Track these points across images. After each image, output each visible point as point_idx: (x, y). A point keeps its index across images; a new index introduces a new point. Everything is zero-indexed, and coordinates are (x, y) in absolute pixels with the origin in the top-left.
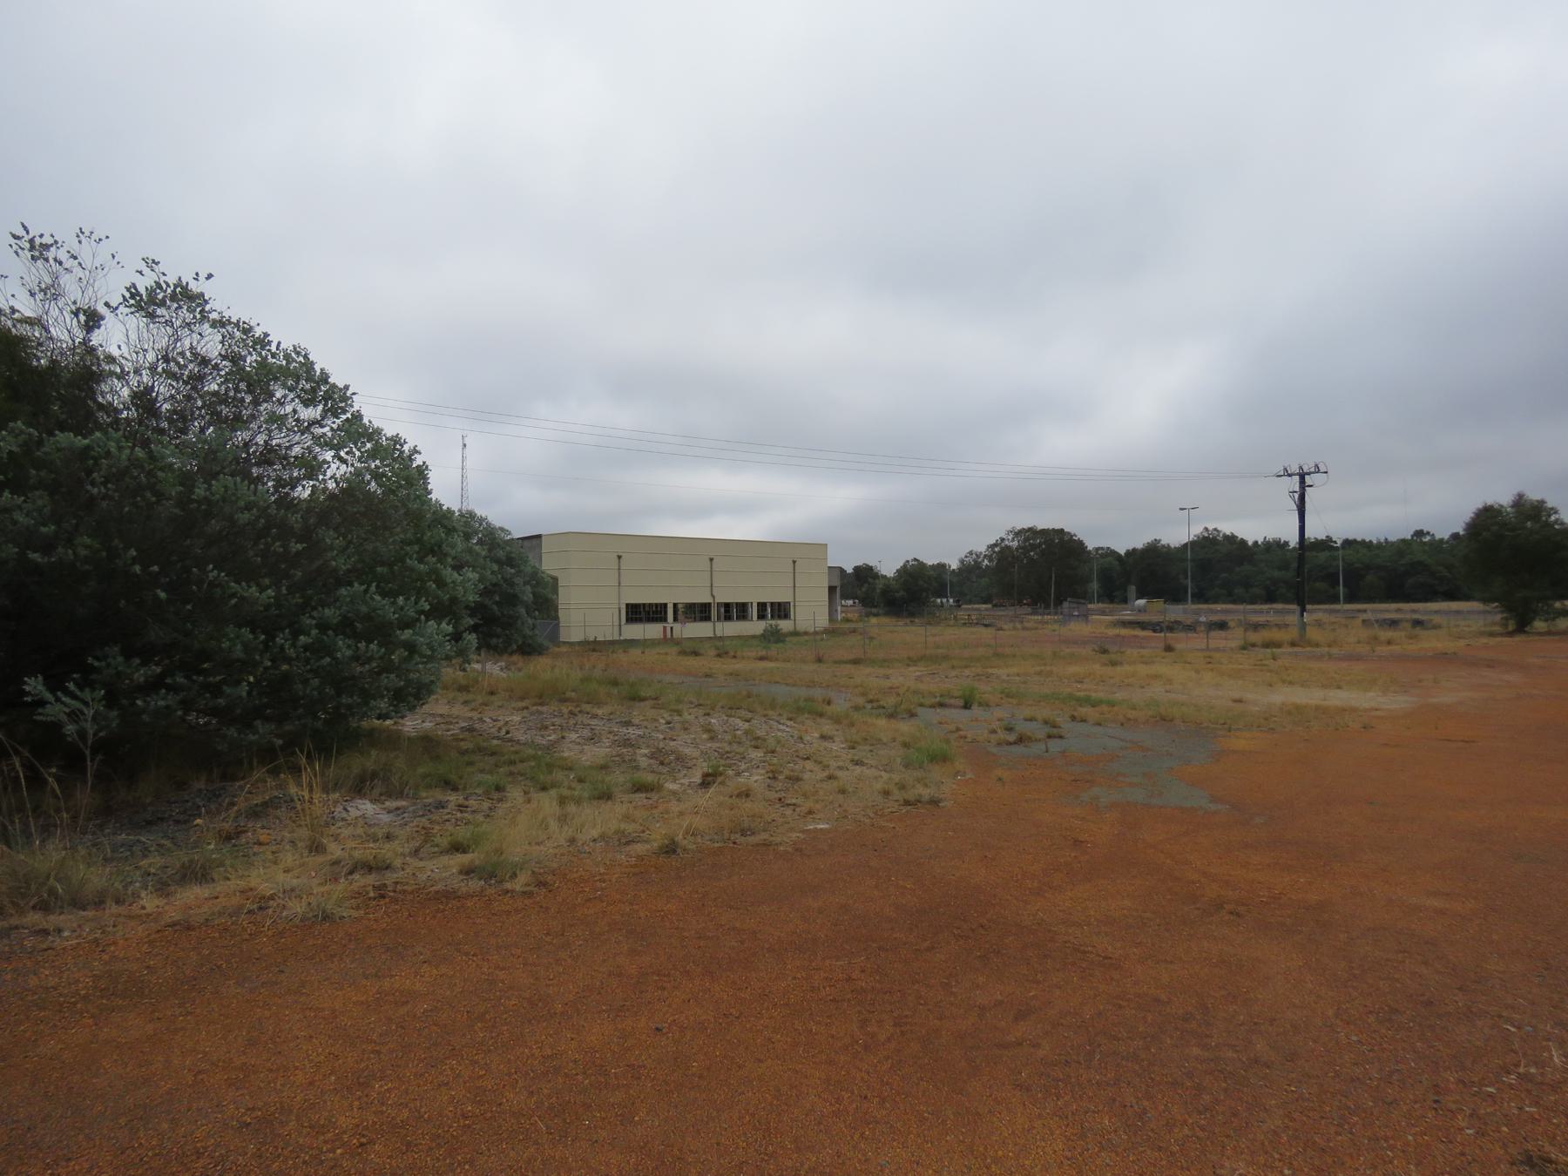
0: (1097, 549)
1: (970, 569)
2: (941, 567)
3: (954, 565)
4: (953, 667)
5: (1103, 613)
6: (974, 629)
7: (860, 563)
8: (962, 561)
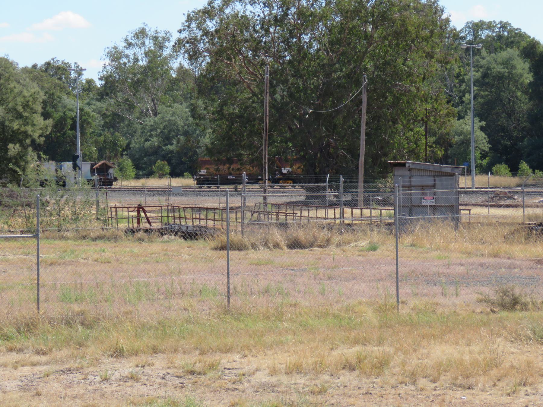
0: (477, 27)
1: (134, 81)
2: (55, 73)
3: (94, 69)
4: (118, 353)
5: (496, 199)
8: (115, 56)
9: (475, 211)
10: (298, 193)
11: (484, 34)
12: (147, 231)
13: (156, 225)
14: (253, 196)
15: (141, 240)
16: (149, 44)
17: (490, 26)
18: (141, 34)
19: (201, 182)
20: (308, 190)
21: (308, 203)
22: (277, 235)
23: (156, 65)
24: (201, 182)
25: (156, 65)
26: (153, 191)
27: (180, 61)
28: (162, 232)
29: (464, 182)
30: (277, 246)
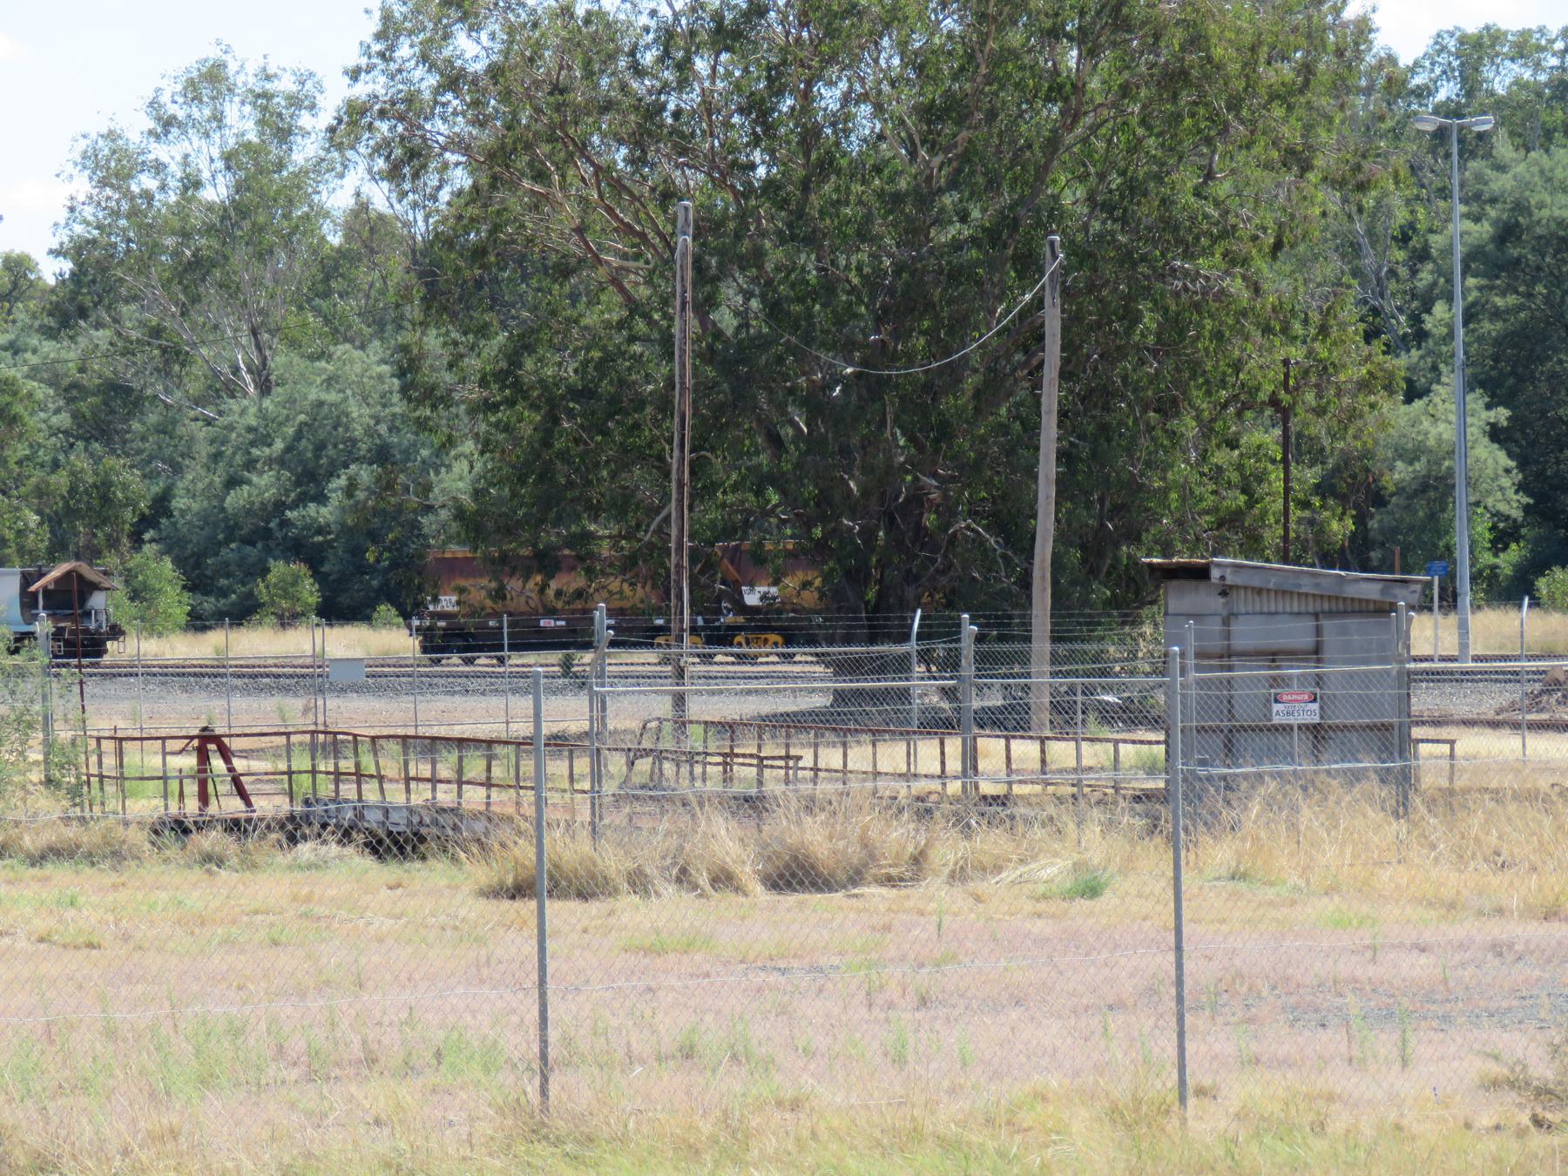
0: (1475, 51)
6: (276, 883)
7: (26, 251)
8: (112, 166)
9: (1472, 743)
10: (805, 681)
11: (1502, 78)
12: (234, 826)
13: (270, 805)
14: (632, 694)
15: (212, 860)
16: (241, 122)
17: (1525, 47)
18: (209, 81)
19: (438, 642)
20: (845, 667)
21: (840, 720)
22: (726, 841)
23: (263, 198)
24: (438, 642)
25: (263, 198)
26: (257, 678)
27: (350, 189)
28: (292, 830)
29: (1429, 635)
30: (723, 879)
